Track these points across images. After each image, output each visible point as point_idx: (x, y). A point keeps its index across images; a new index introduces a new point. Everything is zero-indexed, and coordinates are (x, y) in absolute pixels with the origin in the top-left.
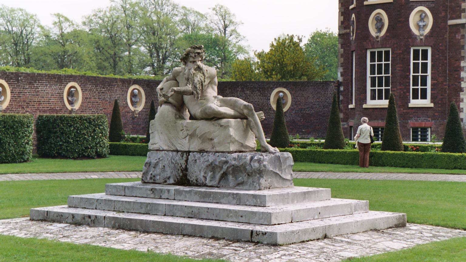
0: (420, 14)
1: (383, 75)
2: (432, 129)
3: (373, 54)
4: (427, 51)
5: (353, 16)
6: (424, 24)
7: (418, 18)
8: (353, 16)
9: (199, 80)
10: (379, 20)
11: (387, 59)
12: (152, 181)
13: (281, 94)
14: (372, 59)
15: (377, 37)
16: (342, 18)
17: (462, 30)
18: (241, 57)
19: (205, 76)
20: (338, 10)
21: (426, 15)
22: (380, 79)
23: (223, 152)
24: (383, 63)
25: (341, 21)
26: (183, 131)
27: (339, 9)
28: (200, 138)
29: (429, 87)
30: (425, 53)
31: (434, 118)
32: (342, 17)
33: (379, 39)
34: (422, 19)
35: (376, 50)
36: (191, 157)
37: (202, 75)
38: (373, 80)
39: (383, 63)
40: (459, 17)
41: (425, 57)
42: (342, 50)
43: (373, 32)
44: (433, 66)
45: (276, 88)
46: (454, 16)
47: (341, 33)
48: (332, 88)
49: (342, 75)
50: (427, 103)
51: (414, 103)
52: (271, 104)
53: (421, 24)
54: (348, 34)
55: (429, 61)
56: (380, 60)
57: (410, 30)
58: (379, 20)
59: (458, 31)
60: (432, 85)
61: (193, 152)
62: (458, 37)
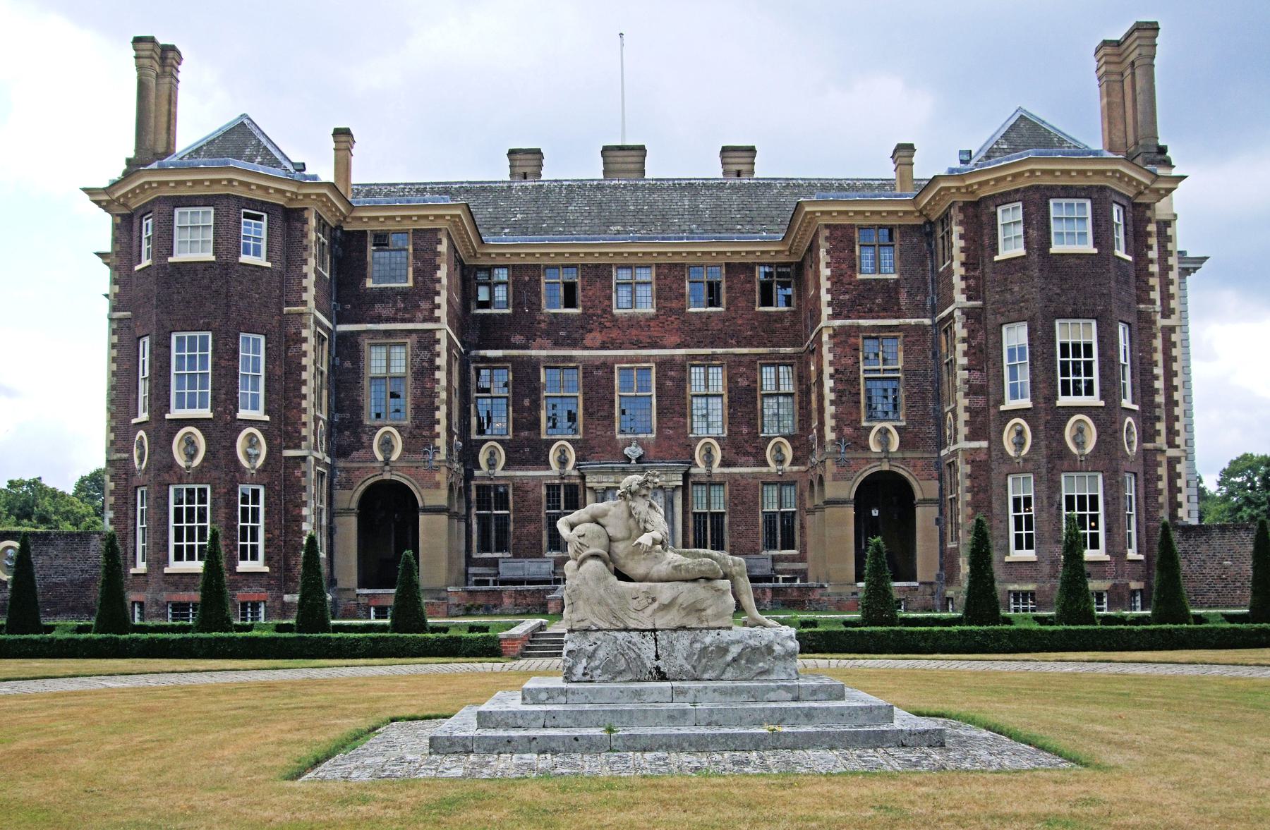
7: (1013, 434)
12: (588, 678)
16: (112, 436)
21: (258, 441)
27: (108, 421)
30: (256, 493)
31: (268, 587)
35: (185, 487)
36: (663, 639)
40: (298, 447)
41: (256, 501)
42: (113, 484)
43: (181, 460)
44: (267, 513)
48: (97, 545)
49: (111, 522)
50: (259, 566)
51: (244, 566)
53: (250, 451)
55: (261, 506)
62: (297, 473)
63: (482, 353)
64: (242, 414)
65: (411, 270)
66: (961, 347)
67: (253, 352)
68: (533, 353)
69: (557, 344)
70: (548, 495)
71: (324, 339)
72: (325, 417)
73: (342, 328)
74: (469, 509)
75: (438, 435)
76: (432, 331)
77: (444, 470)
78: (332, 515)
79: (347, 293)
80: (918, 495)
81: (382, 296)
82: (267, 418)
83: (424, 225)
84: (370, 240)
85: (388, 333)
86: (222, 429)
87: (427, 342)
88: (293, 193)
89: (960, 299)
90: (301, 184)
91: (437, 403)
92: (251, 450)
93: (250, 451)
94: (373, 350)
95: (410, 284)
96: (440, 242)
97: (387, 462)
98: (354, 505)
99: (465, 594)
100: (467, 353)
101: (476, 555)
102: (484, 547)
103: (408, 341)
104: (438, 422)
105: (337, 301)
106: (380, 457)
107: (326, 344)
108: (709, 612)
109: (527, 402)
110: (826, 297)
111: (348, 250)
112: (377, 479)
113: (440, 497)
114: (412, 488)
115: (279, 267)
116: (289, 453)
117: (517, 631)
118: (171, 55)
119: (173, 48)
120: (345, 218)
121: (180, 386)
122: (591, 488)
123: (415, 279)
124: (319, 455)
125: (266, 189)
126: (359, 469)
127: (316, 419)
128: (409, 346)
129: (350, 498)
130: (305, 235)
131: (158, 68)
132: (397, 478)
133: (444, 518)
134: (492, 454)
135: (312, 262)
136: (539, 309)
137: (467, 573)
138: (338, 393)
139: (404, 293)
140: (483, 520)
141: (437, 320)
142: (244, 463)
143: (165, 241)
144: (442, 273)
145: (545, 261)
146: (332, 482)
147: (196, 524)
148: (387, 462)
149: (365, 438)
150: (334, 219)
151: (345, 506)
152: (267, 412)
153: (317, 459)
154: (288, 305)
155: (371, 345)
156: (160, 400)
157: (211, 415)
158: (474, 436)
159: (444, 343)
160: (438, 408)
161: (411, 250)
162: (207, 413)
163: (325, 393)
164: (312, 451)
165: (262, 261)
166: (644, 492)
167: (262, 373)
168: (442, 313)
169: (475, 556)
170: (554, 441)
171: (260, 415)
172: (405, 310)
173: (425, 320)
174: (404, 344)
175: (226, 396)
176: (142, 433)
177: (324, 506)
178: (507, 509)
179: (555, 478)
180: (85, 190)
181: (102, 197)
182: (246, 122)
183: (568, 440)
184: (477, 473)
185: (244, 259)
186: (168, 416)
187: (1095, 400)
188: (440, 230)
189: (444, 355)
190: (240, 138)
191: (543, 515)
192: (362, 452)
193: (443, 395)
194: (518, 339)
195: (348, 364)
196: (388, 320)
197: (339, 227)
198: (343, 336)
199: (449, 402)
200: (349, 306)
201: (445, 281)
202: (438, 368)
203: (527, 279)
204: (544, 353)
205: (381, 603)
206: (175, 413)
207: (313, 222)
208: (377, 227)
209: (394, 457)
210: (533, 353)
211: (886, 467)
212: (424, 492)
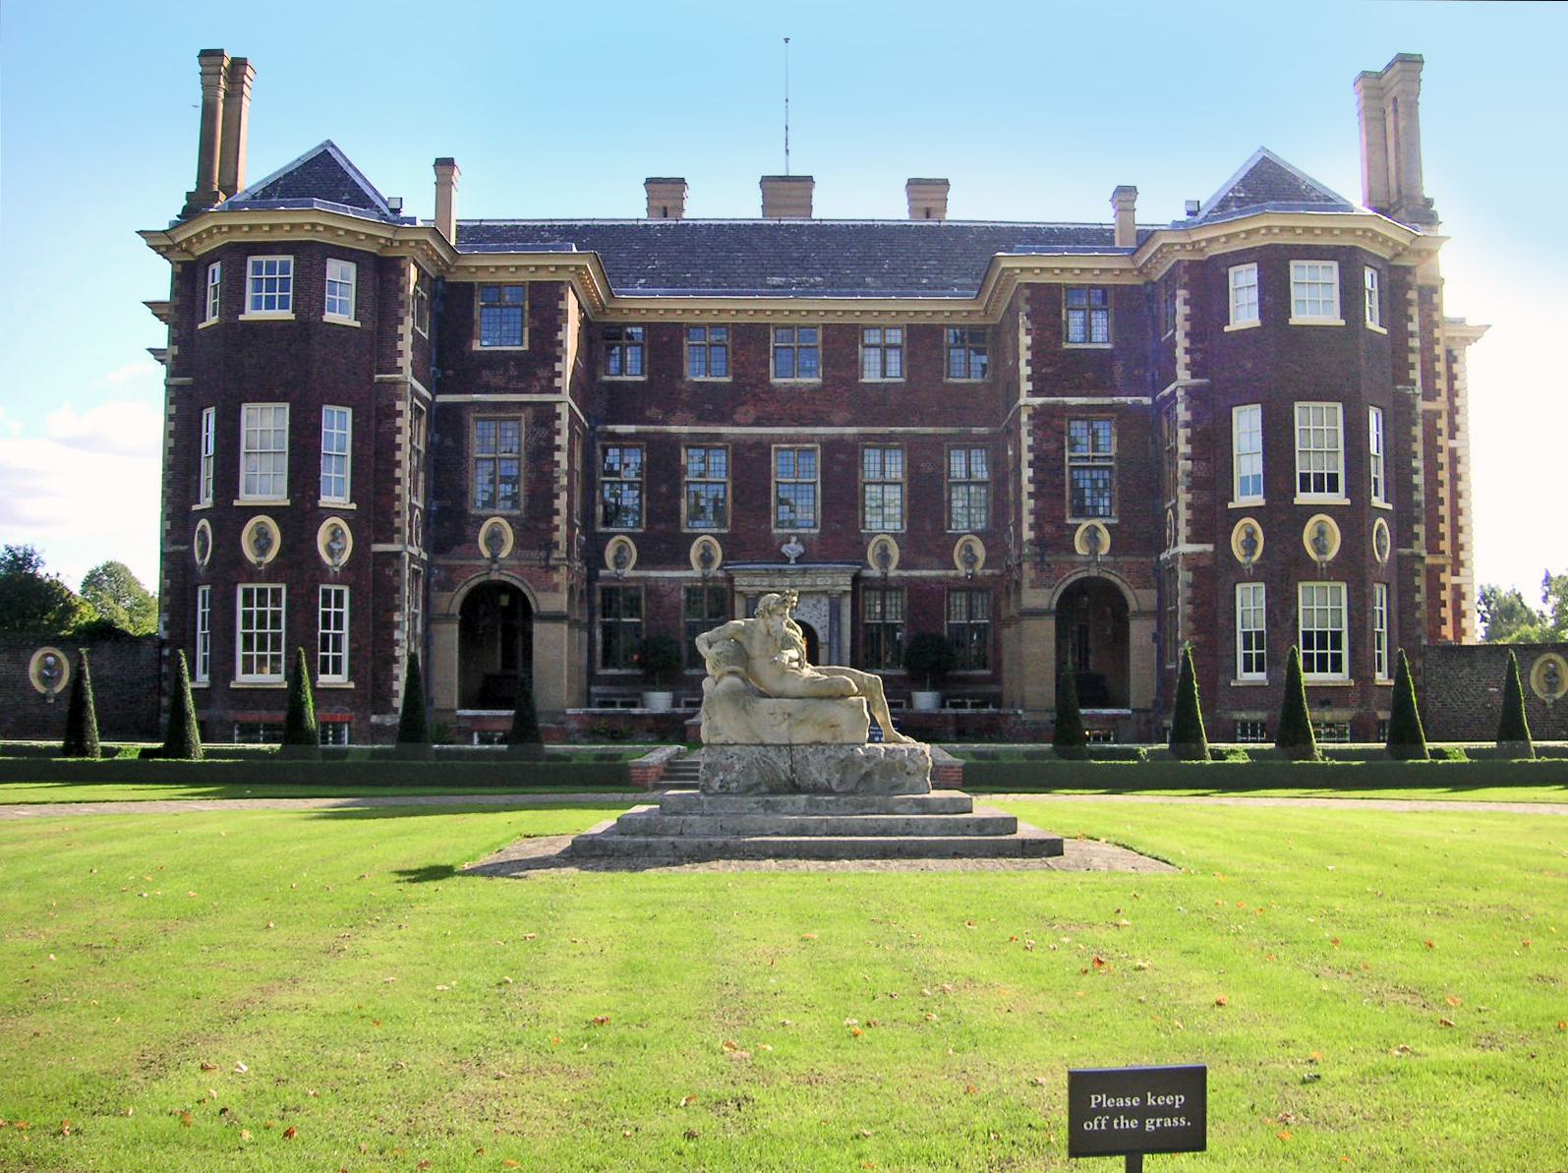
0: (333, 528)
1: (268, 630)
2: (352, 725)
6: (339, 547)
7: (328, 538)
13: (50, 659)
15: (260, 564)
17: (395, 561)
18: (47, 580)
20: (160, 510)
21: (343, 532)
22: (262, 638)
25: (167, 531)
29: (1345, 652)
30: (339, 594)
31: (354, 707)
32: (169, 523)
33: (263, 568)
35: (255, 586)
38: (248, 638)
43: (250, 554)
44: (352, 618)
45: (42, 646)
46: (381, 537)
47: (165, 551)
52: (32, 679)
57: (318, 556)
59: (390, 564)
60: (351, 650)
62: (389, 572)
66: (1183, 433)
67: (338, 426)
68: (673, 429)
69: (702, 419)
71: (421, 412)
73: (441, 398)
74: (592, 615)
76: (552, 404)
77: (564, 570)
79: (449, 359)
80: (1133, 605)
81: (491, 360)
87: (545, 416)
88: (387, 239)
89: (1184, 376)
91: (556, 491)
97: (494, 558)
98: (456, 609)
100: (592, 428)
102: (608, 659)
106: (486, 553)
109: (664, 489)
110: (1025, 370)
111: (452, 304)
112: (483, 579)
115: (369, 326)
122: (741, 592)
127: (412, 507)
129: (452, 602)
132: (508, 579)
134: (620, 550)
135: (409, 321)
136: (681, 376)
137: (589, 691)
140: (609, 632)
141: (558, 390)
143: (233, 297)
146: (432, 583)
148: (494, 558)
149: (469, 531)
159: (565, 418)
160: (557, 496)
173: (542, 391)
176: (204, 522)
177: (419, 611)
179: (697, 580)
181: (159, 242)
183: (711, 535)
184: (602, 573)
187: (1339, 498)
189: (566, 433)
191: (682, 625)
192: (464, 547)
193: (564, 481)
197: (440, 278)
200: (450, 373)
202: (558, 448)
204: (685, 429)
209: (504, 554)
210: (673, 429)
211: (1094, 573)
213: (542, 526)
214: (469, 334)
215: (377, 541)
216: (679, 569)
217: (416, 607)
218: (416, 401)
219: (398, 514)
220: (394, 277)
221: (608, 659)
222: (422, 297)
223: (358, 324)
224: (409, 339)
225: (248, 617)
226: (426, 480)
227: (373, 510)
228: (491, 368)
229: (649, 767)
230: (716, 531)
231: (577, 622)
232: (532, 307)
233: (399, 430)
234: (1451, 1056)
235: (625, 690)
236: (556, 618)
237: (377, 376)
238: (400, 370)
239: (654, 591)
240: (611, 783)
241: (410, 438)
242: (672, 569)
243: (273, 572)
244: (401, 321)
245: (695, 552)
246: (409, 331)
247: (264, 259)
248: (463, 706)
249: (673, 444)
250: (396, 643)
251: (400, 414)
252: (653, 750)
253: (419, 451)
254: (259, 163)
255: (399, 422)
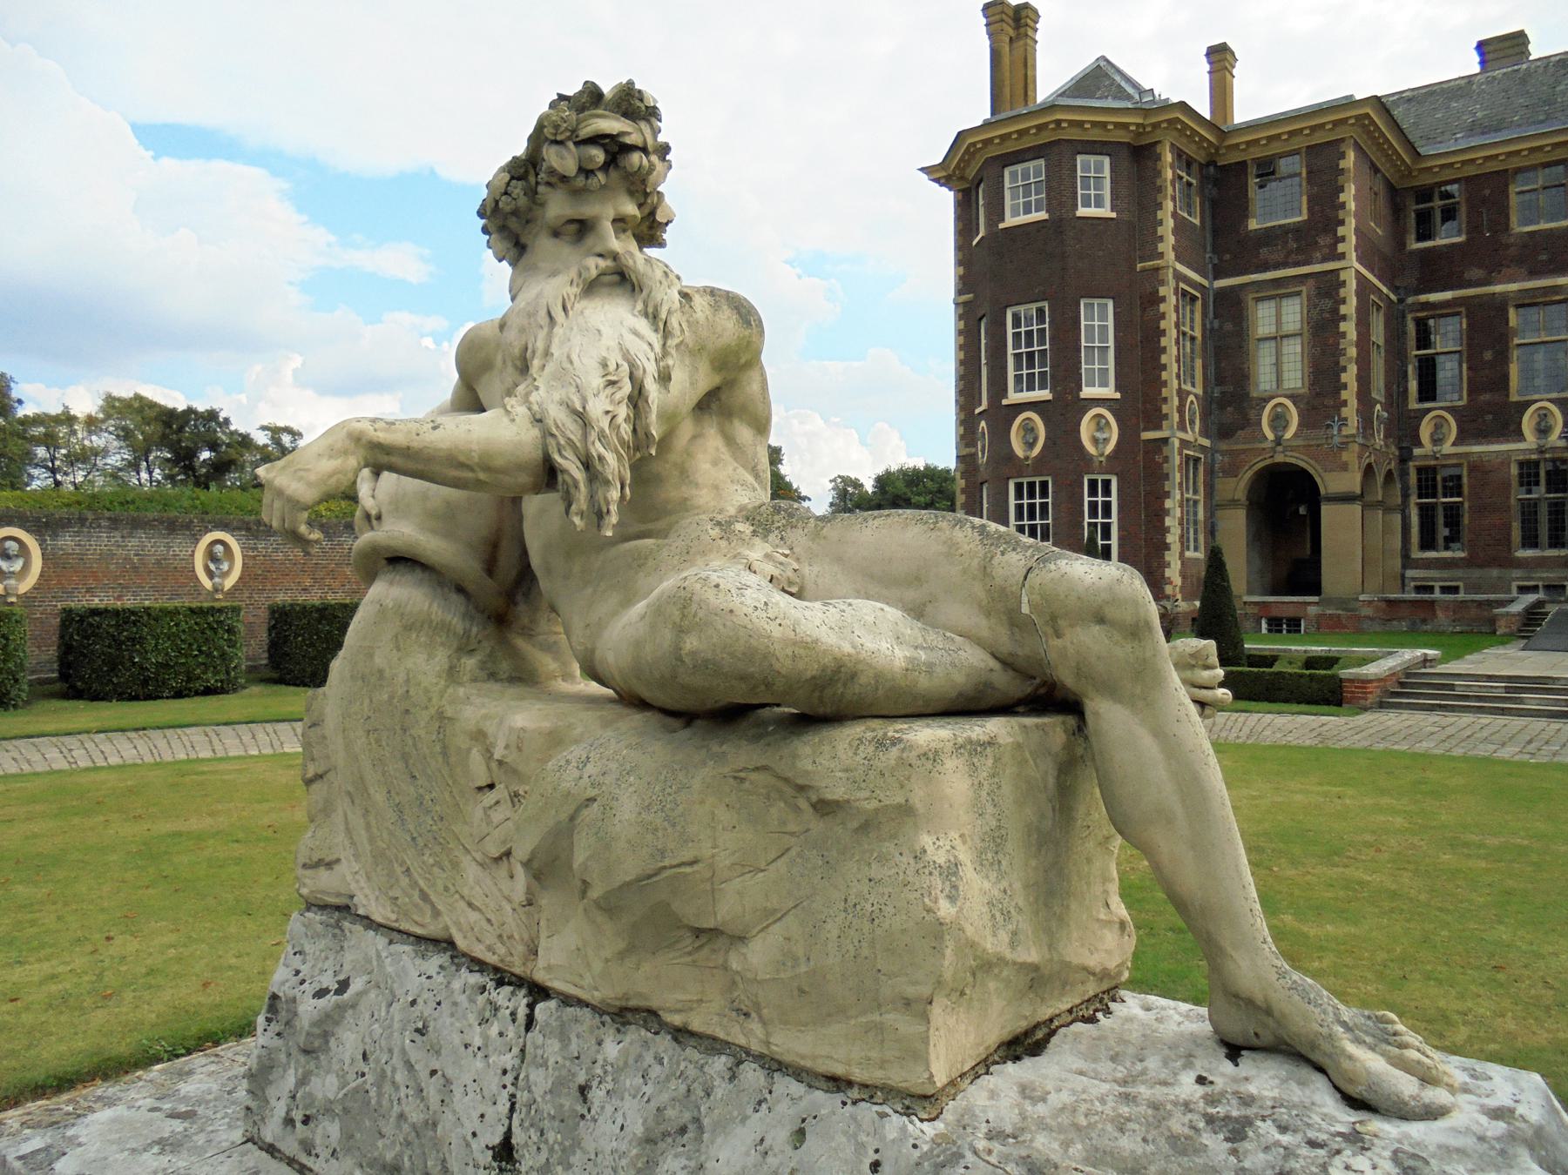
3: (1019, 487)
4: (1421, 399)
5: (983, 424)
7: (1093, 426)
8: (983, 424)
9: (614, 358)
10: (1028, 429)
11: (1044, 494)
14: (1019, 495)
15: (1027, 458)
19: (666, 334)
21: (1108, 422)
23: (837, 1083)
24: (1038, 501)
26: (490, 797)
28: (609, 907)
30: (1107, 484)
34: (1099, 429)
35: (1025, 481)
37: (643, 325)
39: (1038, 501)
40: (1159, 427)
41: (1107, 492)
43: (1019, 450)
53: (1098, 435)
54: (974, 455)
55: (1114, 499)
56: (1032, 495)
57: (1081, 447)
58: (1028, 429)
60: (1120, 538)
61: (567, 1000)
63: (1423, 298)
64: (1087, 392)
65: (1305, 198)
67: (1098, 322)
68: (1498, 288)
69: (1534, 273)
70: (1521, 475)
71: (1193, 299)
72: (1199, 390)
74: (1406, 496)
75: (1345, 403)
76: (1335, 272)
78: (1211, 509)
79: (1226, 238)
81: (1269, 237)
82: (1118, 395)
83: (1320, 138)
84: (1252, 170)
85: (1277, 283)
86: (1064, 411)
87: (1329, 286)
88: (1138, 125)
90: (1146, 112)
91: (1342, 363)
92: (1098, 435)
93: (1098, 435)
94: (1260, 306)
95: (1305, 217)
96: (1343, 156)
99: (1383, 605)
100: (1401, 301)
101: (1417, 554)
102: (1428, 543)
103: (1304, 289)
104: (1345, 386)
105: (1214, 251)
106: (1270, 436)
107: (1199, 304)
108: (758, 955)
109: (1488, 355)
112: (1268, 462)
113: (1351, 481)
114: (1312, 471)
115: (1126, 216)
116: (1148, 435)
117: (1371, 670)
118: (1024, 14)
119: (1026, 6)
120: (1217, 149)
121: (1018, 367)
123: (1310, 209)
124: (1189, 436)
125: (1104, 125)
126: (1244, 451)
127: (1183, 395)
128: (1304, 294)
129: (1237, 487)
130: (1158, 173)
131: (1012, 32)
132: (1293, 461)
133: (1357, 508)
134: (1437, 427)
135: (1169, 205)
136: (1507, 227)
137: (1403, 576)
138: (1218, 362)
139: (1296, 230)
140: (1427, 513)
141: (1342, 256)
142: (1091, 449)
143: (997, 212)
144: (1349, 197)
145: (1515, 163)
146: (1207, 469)
147: (1026, 522)
149: (1252, 414)
150: (1203, 153)
151: (1230, 497)
152: (1118, 388)
153: (1182, 440)
154: (1142, 260)
155: (1258, 300)
156: (999, 388)
157: (1050, 397)
158: (1414, 405)
159: (1352, 285)
160: (1344, 369)
161: (1304, 175)
162: (1045, 394)
163: (1199, 363)
164: (1181, 432)
165: (1105, 212)
166: (557, 207)
167: (1111, 343)
168: (1349, 246)
169: (1414, 556)
170: (1528, 404)
171: (1109, 392)
172: (1299, 250)
173: (1324, 260)
174: (1298, 294)
175: (1066, 373)
177: (1200, 497)
178: (1459, 495)
179: (1531, 451)
180: (922, 169)
182: (1102, 64)
183: (1550, 400)
184: (1417, 451)
185: (1082, 211)
186: (1004, 402)
188: (1343, 140)
189: (1353, 301)
190: (1100, 77)
191: (1513, 501)
192: (1248, 430)
193: (1353, 352)
194: (1476, 273)
195: (1229, 326)
196: (1277, 267)
197: (1211, 163)
198: (1222, 294)
199: (1364, 363)
200: (1228, 257)
201: (1352, 206)
202: (1344, 318)
203: (1487, 192)
204: (1513, 287)
205: (1275, 613)
206: (1013, 397)
207: (1168, 157)
208: (1257, 153)
209: (1289, 435)
210: (1498, 288)
212: (1327, 476)
213: (1329, 402)
214: (1244, 214)
215: (1146, 429)
216: (1508, 441)
217: (1195, 492)
218: (1182, 285)
219: (1165, 400)
220: (1150, 164)
221: (1428, 543)
222: (1189, 184)
223: (1114, 215)
224: (1170, 223)
225: (1107, 513)
226: (1204, 367)
227: (1140, 400)
228: (1267, 245)
229: (1370, 681)
230: (1554, 395)
231: (1380, 504)
232: (1309, 173)
233: (1163, 316)
234: (1268, 369)
235: (1445, 574)
236: (1347, 498)
237: (1139, 266)
238: (1161, 255)
239: (1478, 468)
240: (1328, 702)
241: (1179, 328)
242: (1498, 442)
243: (1040, 464)
244: (1160, 206)
245: (1528, 422)
246: (1171, 214)
247: (1019, 168)
248: (1250, 593)
249: (1498, 307)
250: (1167, 530)
251: (1163, 299)
252: (1390, 653)
253: (1193, 339)
254: (1052, 74)
255: (1163, 307)
